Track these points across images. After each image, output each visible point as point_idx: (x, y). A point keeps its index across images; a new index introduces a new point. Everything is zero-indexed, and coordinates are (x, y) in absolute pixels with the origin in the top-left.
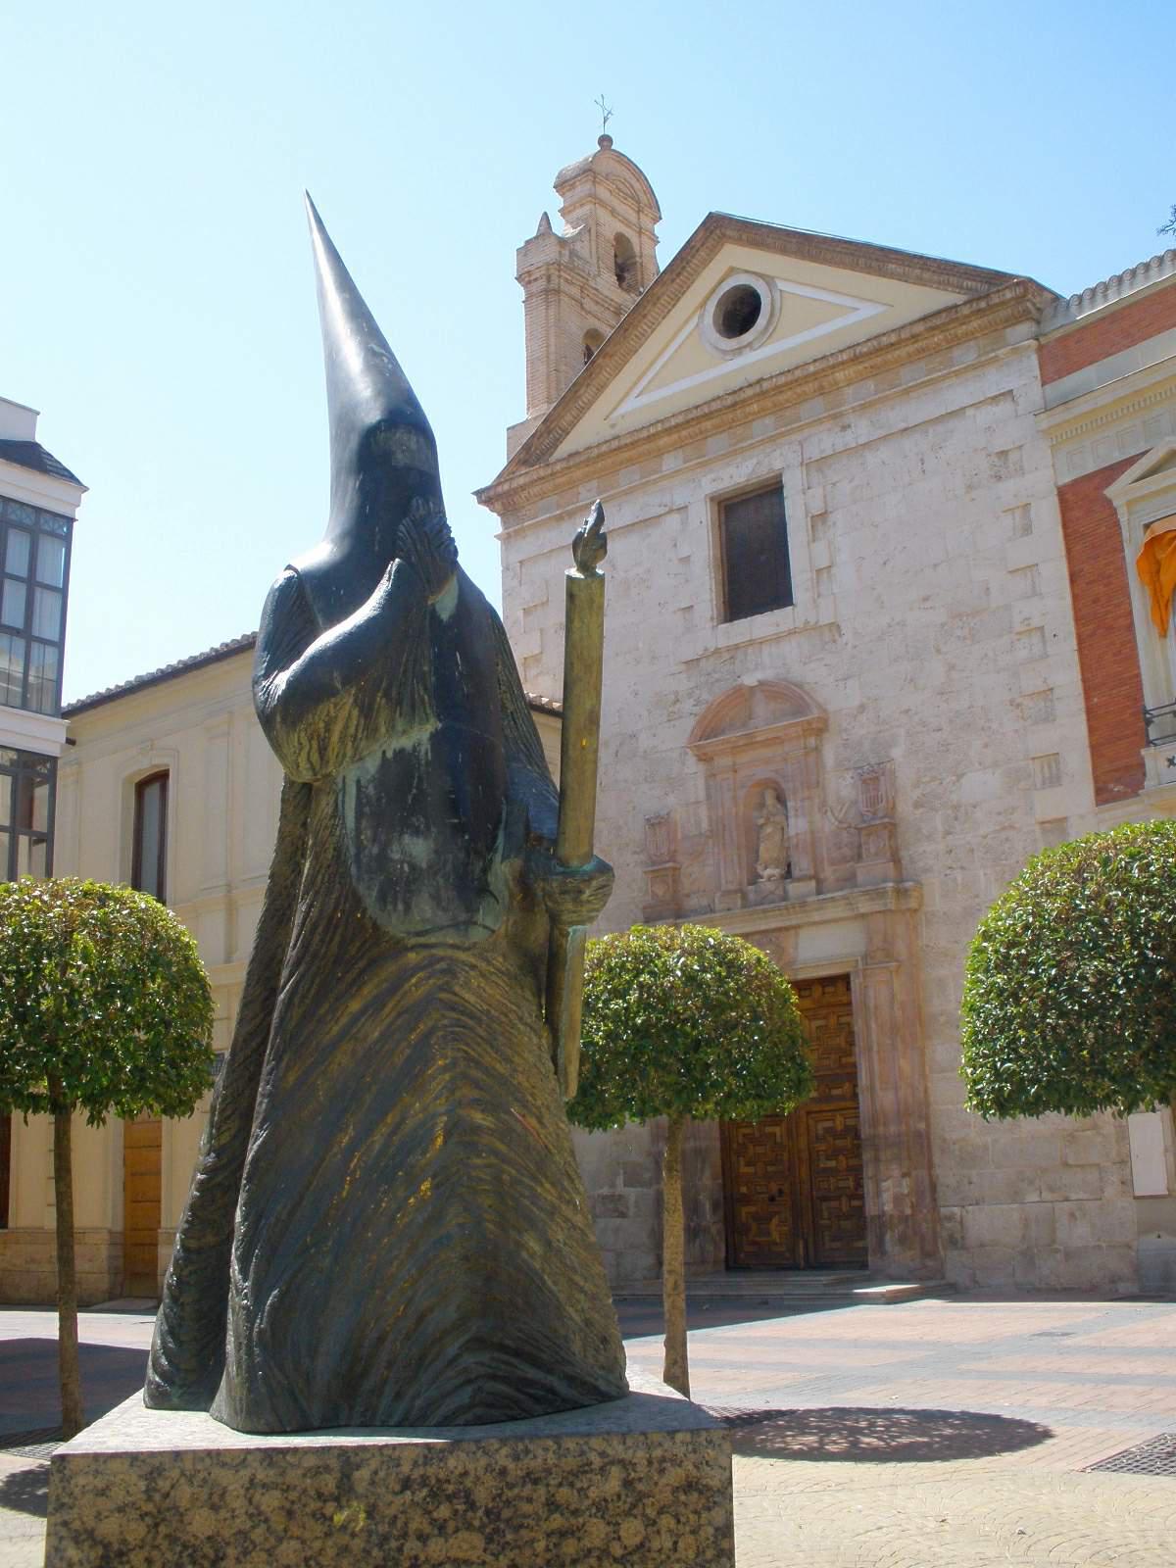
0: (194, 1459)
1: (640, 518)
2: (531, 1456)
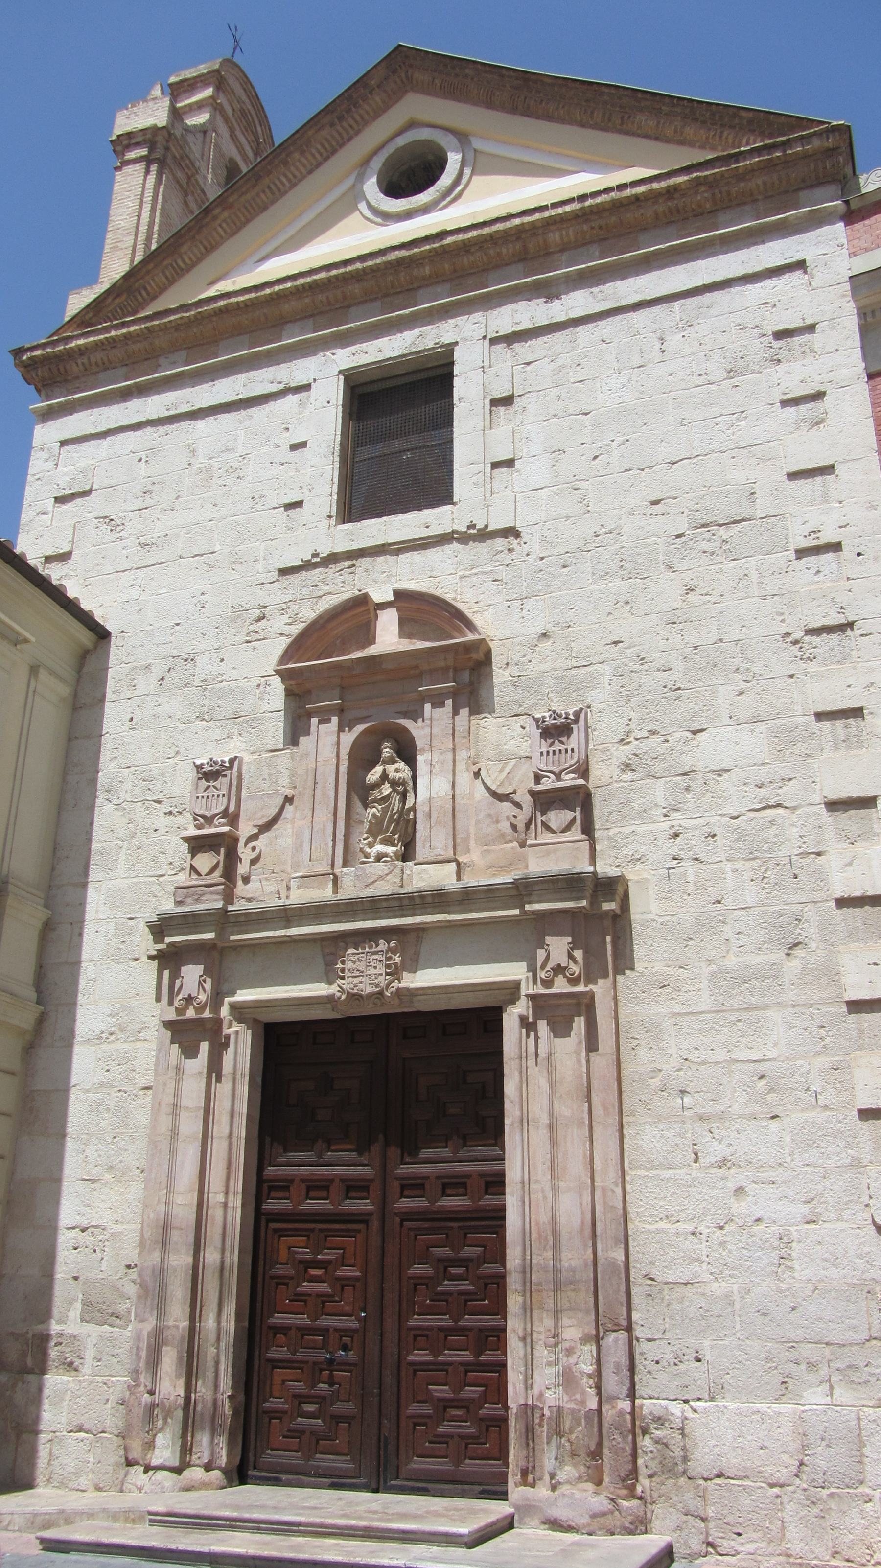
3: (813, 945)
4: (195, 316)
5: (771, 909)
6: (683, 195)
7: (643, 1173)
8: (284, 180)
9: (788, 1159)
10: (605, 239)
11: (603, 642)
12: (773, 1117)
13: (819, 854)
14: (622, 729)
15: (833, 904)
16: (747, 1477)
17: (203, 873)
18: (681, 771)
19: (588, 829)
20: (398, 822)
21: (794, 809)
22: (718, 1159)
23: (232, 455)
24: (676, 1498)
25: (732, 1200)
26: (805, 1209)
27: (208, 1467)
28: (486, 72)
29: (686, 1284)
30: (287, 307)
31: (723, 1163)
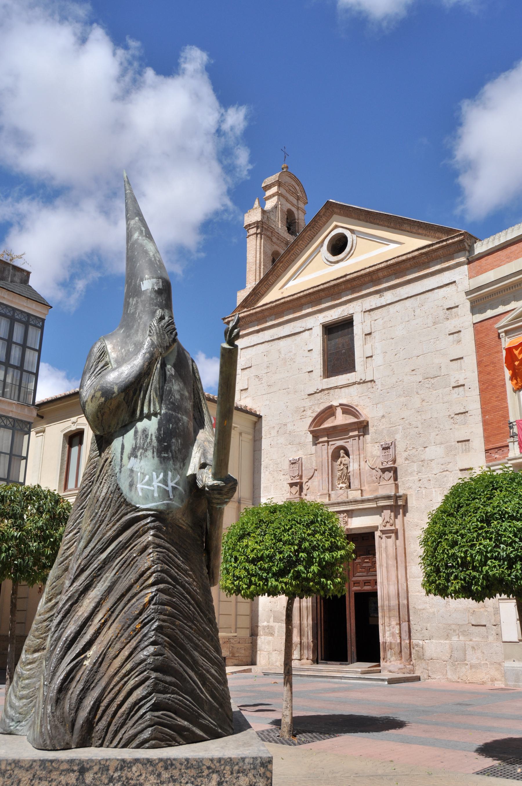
0: (7, 763)
1: (292, 333)
2: (174, 767)
14: (405, 447)
18: (421, 460)
19: (396, 479)
21: (451, 472)
23: (292, 354)
27: (307, 659)
30: (303, 301)
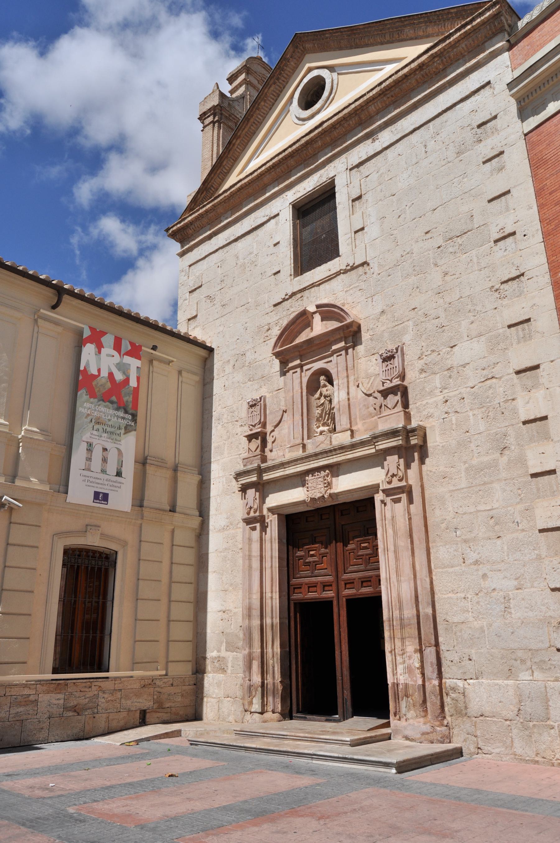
3: (513, 447)
4: (230, 194)
5: (492, 432)
6: (428, 66)
7: (441, 570)
8: (260, 117)
9: (506, 558)
10: (396, 101)
11: (408, 310)
12: (498, 537)
13: (513, 400)
15: (521, 424)
16: (494, 716)
17: (253, 451)
18: (447, 368)
19: (406, 405)
20: (329, 414)
22: (474, 560)
23: (252, 255)
24: (462, 727)
25: (481, 580)
26: (516, 583)
28: (335, 33)
29: (462, 623)
31: (476, 562)
